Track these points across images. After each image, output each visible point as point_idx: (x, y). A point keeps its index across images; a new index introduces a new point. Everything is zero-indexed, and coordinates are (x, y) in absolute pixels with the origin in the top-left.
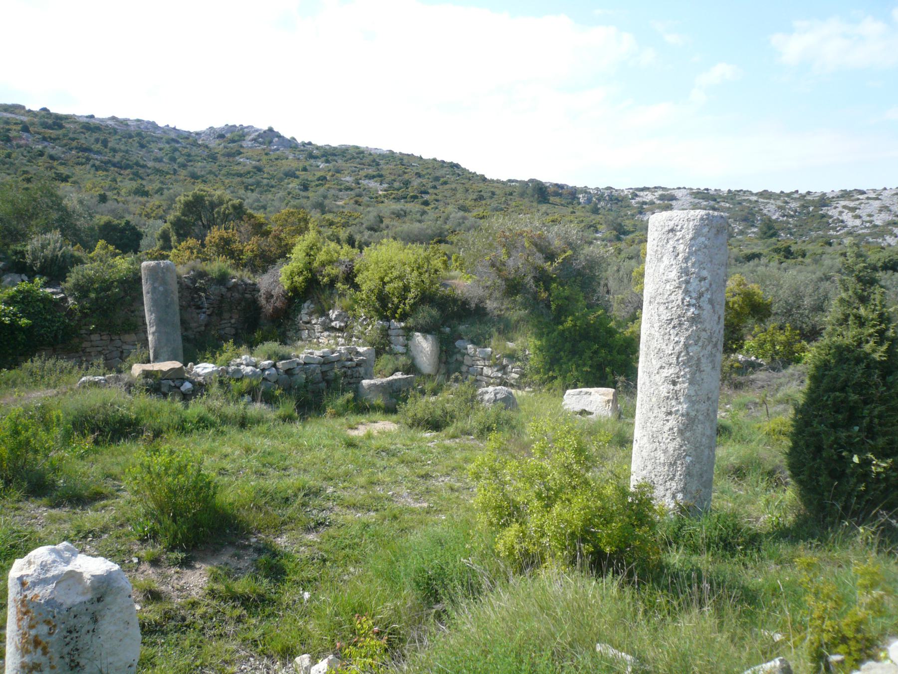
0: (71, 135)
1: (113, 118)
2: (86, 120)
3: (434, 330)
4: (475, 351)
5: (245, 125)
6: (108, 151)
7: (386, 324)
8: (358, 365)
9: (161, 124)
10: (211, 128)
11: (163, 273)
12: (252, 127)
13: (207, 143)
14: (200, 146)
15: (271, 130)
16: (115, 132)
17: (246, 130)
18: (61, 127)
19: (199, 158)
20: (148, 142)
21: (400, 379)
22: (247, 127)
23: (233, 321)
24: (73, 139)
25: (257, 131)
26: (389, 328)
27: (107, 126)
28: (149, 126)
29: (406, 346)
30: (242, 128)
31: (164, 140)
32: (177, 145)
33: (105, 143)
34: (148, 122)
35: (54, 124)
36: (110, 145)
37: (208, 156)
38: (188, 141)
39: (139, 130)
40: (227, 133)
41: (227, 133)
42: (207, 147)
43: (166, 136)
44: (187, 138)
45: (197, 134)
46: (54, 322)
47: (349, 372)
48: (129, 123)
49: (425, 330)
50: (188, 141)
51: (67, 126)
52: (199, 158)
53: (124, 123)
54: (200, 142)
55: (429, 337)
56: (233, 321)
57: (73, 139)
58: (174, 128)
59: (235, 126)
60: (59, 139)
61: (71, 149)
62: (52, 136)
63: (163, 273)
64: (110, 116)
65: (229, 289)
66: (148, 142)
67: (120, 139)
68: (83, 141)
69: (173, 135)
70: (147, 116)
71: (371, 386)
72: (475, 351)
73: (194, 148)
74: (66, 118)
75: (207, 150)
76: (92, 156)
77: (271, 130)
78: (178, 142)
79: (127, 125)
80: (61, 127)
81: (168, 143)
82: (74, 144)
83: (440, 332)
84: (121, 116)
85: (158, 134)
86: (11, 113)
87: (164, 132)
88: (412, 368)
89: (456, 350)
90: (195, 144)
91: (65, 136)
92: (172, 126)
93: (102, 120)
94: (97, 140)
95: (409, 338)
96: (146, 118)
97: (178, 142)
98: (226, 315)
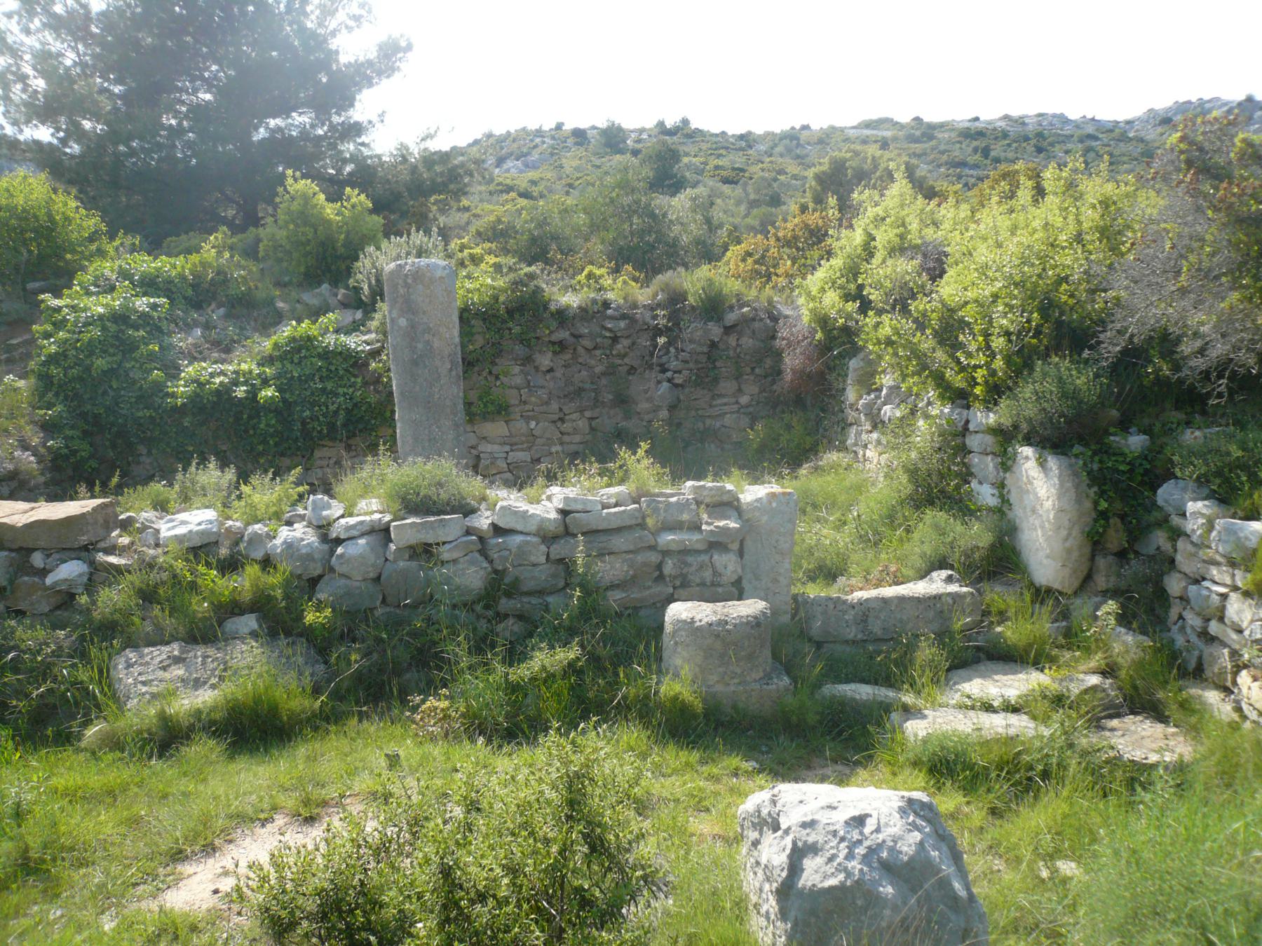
0: (942, 147)
1: (1006, 117)
2: (967, 125)
3: (1082, 440)
4: (1210, 526)
5: (1206, 98)
6: (988, 162)
7: (958, 415)
8: (716, 544)
9: (1074, 115)
10: (1151, 110)
11: (407, 286)
12: (1218, 99)
13: (1142, 134)
14: (1131, 139)
15: (1250, 99)
16: (1005, 135)
17: (1207, 106)
18: (931, 138)
19: (1125, 159)
20: (1052, 144)
21: (937, 598)
22: (1209, 101)
23: (744, 400)
24: (942, 153)
25: (1226, 104)
26: (966, 429)
27: (995, 129)
28: (1055, 121)
29: (1001, 486)
30: (1201, 102)
31: (1075, 138)
32: (1094, 144)
33: (986, 152)
34: (1054, 116)
35: (924, 135)
36: (993, 154)
37: (1142, 154)
38: (1113, 135)
39: (1040, 129)
40: (1175, 114)
41: (1175, 114)
42: (1142, 140)
43: (1079, 132)
44: (1111, 131)
45: (1128, 122)
46: (337, 395)
47: (669, 568)
48: (1027, 121)
49: (1054, 439)
50: (1113, 135)
51: (940, 136)
52: (1125, 159)
53: (1021, 122)
54: (1131, 135)
55: (1053, 462)
56: (744, 400)
57: (942, 153)
58: (1093, 119)
59: (1189, 102)
60: (925, 154)
61: (939, 166)
62: (917, 151)
63: (407, 286)
64: (1001, 115)
65: (728, 330)
66: (1052, 144)
67: (1009, 145)
68: (956, 154)
69: (1090, 130)
70: (1051, 107)
71: (689, 626)
72: (1210, 526)
73: (1122, 144)
74: (942, 126)
75: (1141, 145)
76: (967, 171)
77: (1250, 99)
78: (1096, 138)
79: (1024, 124)
80: (931, 138)
81: (1081, 141)
82: (945, 157)
83: (1105, 451)
84: (1015, 113)
85: (1068, 130)
86: (873, 129)
87: (1077, 127)
88: (1000, 562)
89: (1156, 515)
90: (1123, 138)
91: (933, 149)
92: (1089, 116)
93: (989, 123)
94: (976, 150)
95: (1007, 462)
96: (1050, 109)
97: (1096, 138)
98: (727, 386)
